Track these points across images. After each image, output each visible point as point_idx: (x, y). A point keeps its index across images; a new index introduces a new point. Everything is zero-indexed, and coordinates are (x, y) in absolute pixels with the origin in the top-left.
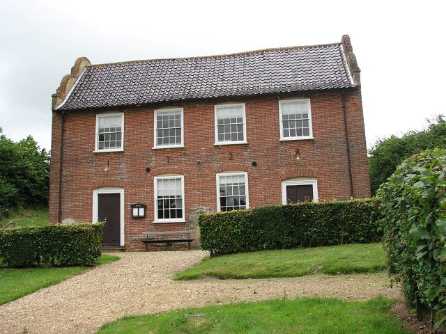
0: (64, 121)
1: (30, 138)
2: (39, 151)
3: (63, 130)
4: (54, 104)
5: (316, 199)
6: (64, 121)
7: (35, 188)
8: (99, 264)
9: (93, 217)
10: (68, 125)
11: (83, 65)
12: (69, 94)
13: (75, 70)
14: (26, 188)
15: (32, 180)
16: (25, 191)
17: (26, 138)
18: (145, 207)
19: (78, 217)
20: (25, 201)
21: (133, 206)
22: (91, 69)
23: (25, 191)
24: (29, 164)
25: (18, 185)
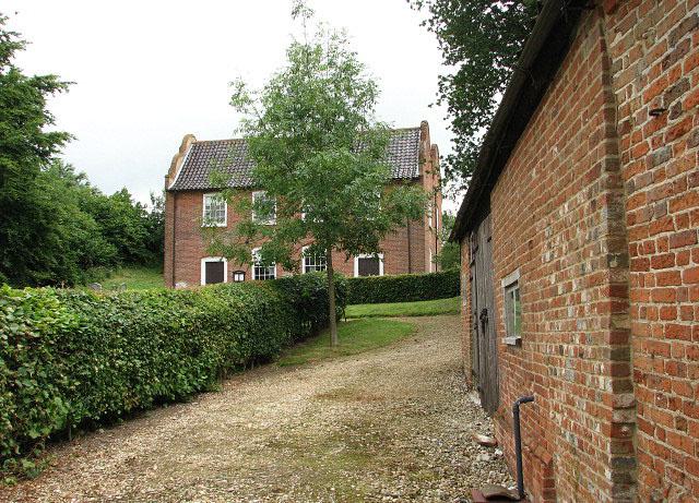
0: (175, 199)
1: (124, 191)
2: (134, 205)
3: (175, 207)
4: (167, 183)
5: (381, 274)
6: (175, 199)
7: (133, 246)
8: (215, 391)
9: (400, 304)
10: (179, 202)
11: (189, 142)
12: (178, 173)
13: (182, 149)
14: (125, 246)
15: (130, 239)
16: (124, 250)
17: (120, 191)
18: (244, 273)
19: (188, 281)
20: (124, 260)
21: (235, 273)
22: (198, 146)
23: (124, 250)
24: (128, 222)
25: (117, 244)
